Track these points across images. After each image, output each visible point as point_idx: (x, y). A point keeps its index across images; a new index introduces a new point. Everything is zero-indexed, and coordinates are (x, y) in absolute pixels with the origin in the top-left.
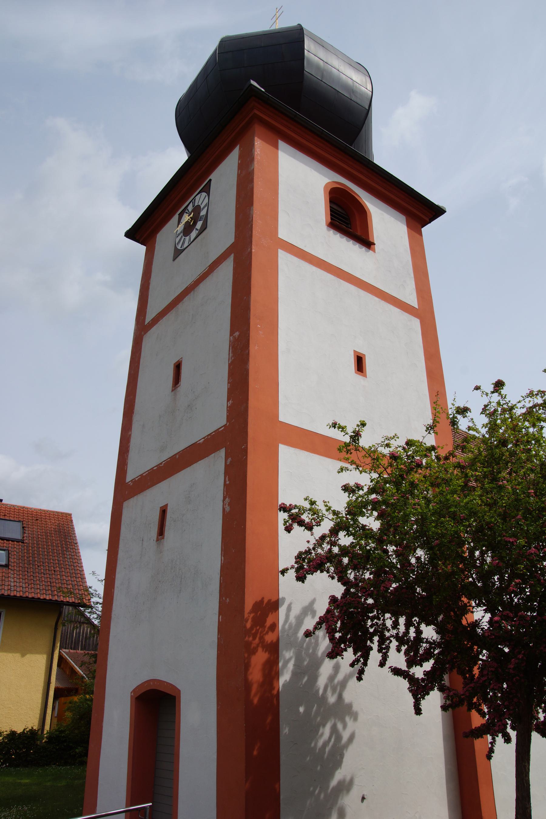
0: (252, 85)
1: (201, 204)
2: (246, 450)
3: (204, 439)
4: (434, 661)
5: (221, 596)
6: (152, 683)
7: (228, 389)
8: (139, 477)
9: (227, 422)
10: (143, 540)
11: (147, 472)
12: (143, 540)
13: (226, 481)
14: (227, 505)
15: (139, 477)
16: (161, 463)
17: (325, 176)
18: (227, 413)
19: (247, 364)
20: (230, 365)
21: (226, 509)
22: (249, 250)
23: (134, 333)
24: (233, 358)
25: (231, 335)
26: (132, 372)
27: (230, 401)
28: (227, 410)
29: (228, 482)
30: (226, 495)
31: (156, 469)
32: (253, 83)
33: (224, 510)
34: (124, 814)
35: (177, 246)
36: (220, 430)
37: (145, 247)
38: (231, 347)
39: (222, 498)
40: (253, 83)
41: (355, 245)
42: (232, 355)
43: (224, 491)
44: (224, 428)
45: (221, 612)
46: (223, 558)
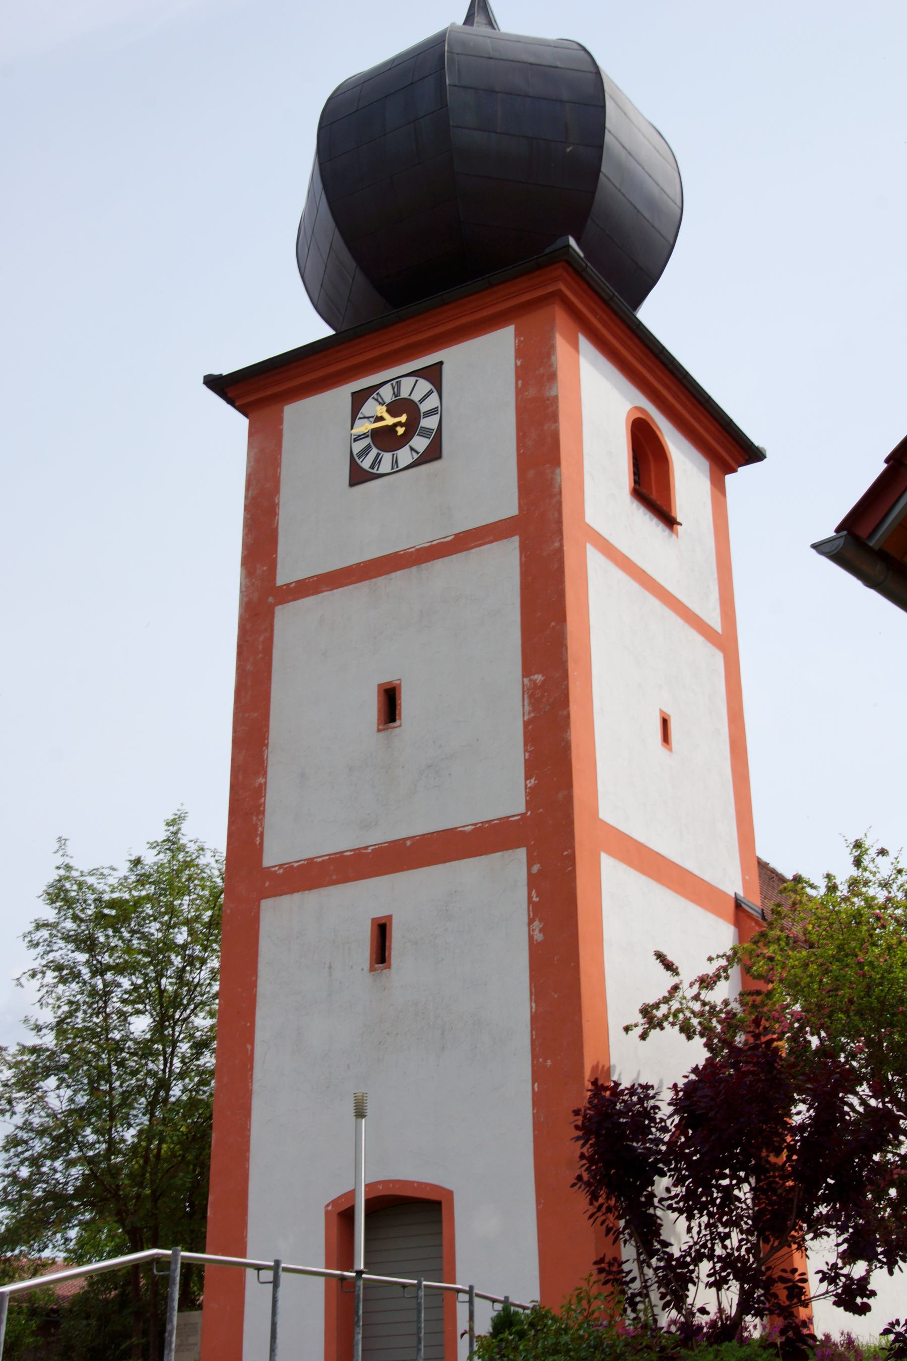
0: (569, 246)
1: (422, 401)
2: (572, 859)
3: (473, 827)
4: (849, 1096)
5: (534, 1056)
6: (391, 1185)
7: (526, 760)
8: (302, 862)
9: (527, 809)
10: (330, 968)
11: (327, 857)
12: (330, 968)
13: (532, 898)
14: (537, 932)
15: (302, 862)
16: (366, 848)
17: (507, 325)
18: (526, 796)
19: (567, 732)
20: (526, 724)
21: (535, 937)
22: (557, 544)
23: (241, 592)
24: (532, 715)
25: (524, 676)
26: (249, 667)
27: (533, 780)
28: (526, 792)
29: (535, 899)
30: (533, 916)
31: (351, 855)
32: (572, 242)
33: (531, 938)
34: (322, 1280)
35: (359, 461)
36: (511, 819)
37: (522, 809)
38: (526, 696)
39: (525, 919)
40: (572, 242)
41: (658, 526)
42: (531, 709)
43: (529, 911)
44: (519, 817)
45: (536, 1076)
46: (534, 1005)
